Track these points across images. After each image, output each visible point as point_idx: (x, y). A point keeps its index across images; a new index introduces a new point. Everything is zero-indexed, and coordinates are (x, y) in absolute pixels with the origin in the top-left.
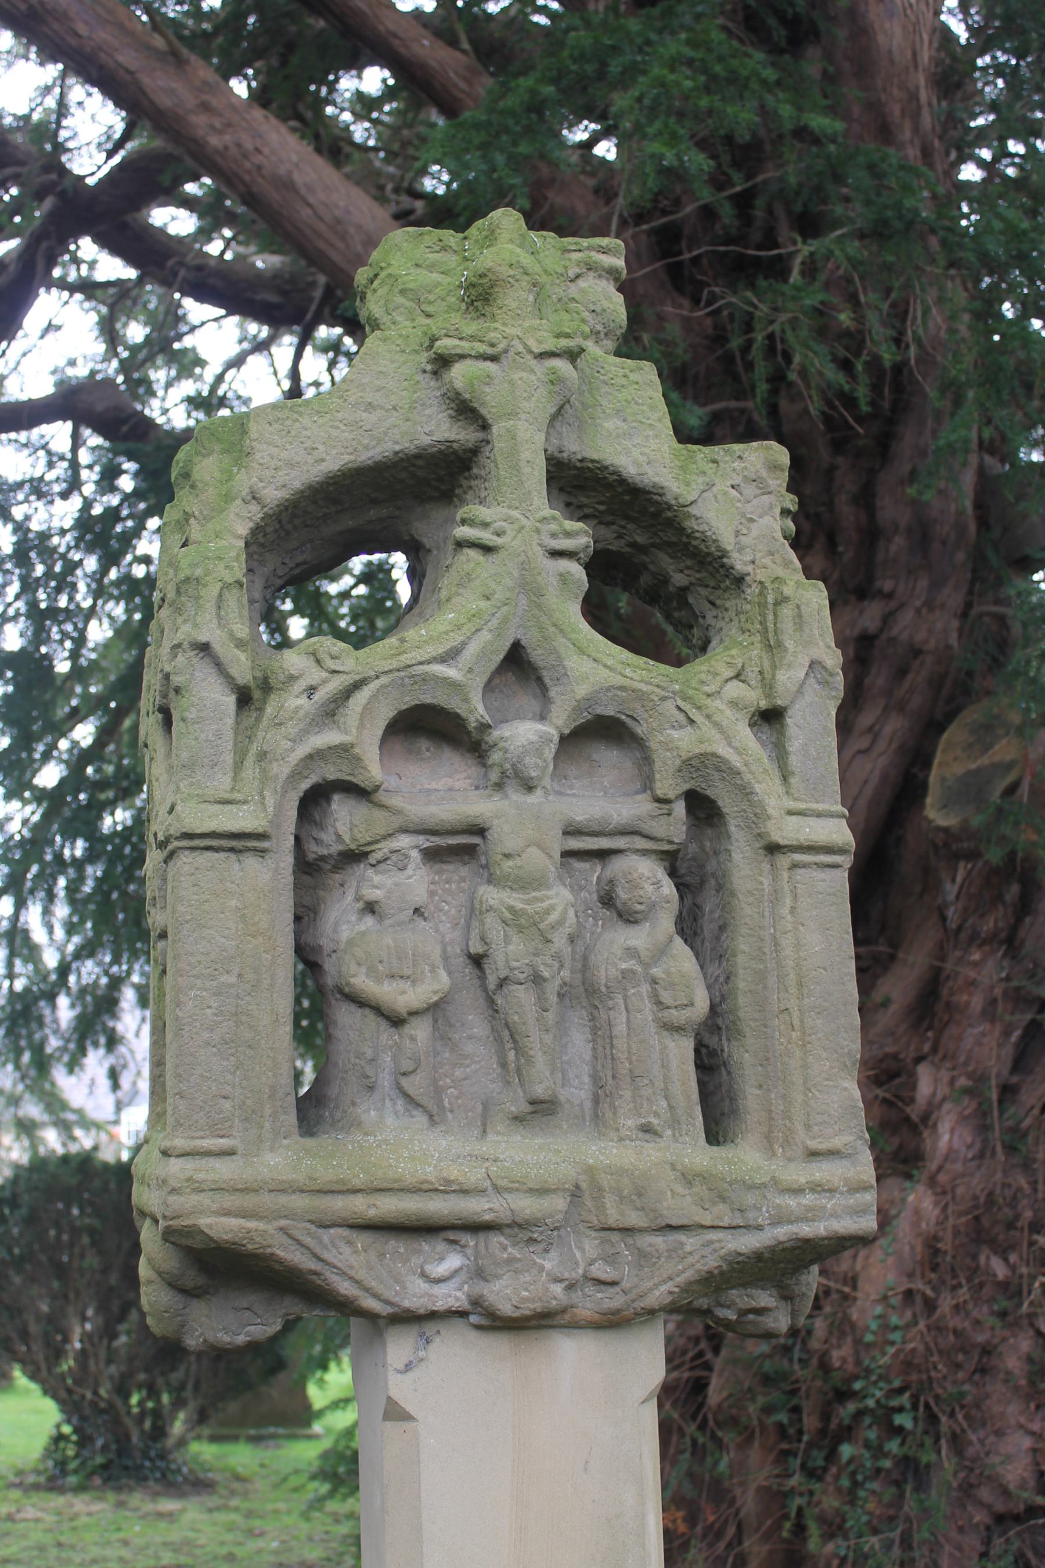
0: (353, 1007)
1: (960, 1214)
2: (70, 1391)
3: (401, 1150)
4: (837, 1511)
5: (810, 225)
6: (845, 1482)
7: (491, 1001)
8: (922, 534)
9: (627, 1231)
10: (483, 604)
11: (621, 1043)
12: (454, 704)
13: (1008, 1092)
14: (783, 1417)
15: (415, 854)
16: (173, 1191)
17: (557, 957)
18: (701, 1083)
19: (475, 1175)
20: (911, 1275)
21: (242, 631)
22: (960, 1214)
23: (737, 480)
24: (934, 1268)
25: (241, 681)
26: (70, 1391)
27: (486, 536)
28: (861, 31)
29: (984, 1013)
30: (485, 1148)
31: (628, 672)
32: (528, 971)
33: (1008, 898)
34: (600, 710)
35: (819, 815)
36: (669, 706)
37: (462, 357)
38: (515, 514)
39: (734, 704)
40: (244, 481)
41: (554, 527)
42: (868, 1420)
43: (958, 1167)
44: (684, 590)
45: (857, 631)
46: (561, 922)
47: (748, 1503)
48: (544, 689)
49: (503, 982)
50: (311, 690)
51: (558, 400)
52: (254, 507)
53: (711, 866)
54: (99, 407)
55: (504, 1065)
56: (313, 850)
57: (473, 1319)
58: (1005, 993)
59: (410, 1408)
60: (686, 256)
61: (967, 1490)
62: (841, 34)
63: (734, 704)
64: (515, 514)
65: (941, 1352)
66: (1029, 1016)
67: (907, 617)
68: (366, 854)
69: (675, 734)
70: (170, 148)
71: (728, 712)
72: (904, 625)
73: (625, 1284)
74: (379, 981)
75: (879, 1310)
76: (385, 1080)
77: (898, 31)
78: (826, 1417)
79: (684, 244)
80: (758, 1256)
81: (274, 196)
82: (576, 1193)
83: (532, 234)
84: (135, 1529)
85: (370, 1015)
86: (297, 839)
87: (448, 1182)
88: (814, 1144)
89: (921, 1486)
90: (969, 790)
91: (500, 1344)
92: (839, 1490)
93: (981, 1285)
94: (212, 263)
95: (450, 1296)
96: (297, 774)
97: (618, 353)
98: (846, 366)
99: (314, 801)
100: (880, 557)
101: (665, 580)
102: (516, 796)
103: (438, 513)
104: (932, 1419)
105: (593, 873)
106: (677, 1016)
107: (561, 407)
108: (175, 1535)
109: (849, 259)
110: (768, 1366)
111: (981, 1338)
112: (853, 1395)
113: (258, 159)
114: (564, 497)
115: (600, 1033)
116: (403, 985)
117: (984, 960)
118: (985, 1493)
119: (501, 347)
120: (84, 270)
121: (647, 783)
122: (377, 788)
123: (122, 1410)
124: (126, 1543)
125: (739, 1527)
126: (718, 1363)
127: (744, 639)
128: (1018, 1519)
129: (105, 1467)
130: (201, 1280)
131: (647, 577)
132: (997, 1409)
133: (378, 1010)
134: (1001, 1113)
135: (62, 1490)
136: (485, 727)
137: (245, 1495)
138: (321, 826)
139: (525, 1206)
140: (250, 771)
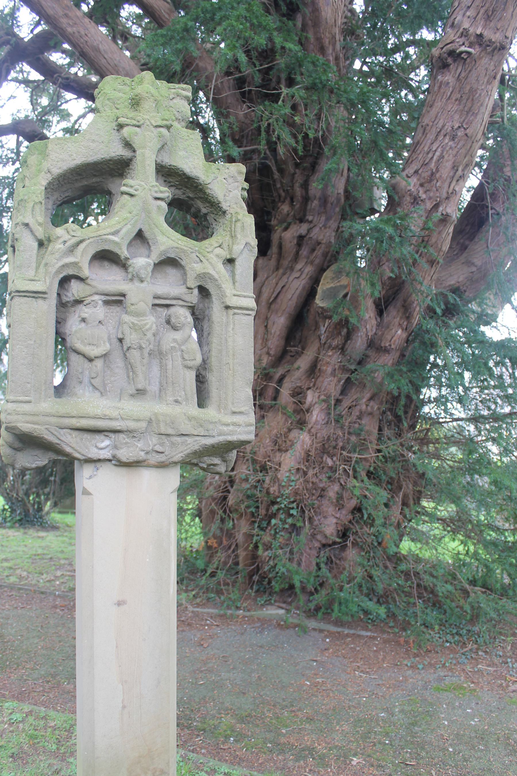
0: (76, 354)
1: (318, 443)
2: (8, 494)
3: (91, 404)
4: (269, 542)
5: (291, 82)
6: (273, 532)
7: (125, 355)
8: (324, 201)
9: (168, 435)
10: (129, 215)
11: (169, 372)
12: (116, 250)
13: (338, 402)
14: (253, 510)
15: (100, 302)
16: (9, 414)
17: (148, 340)
18: (197, 386)
19: (115, 414)
20: (299, 463)
21: (41, 219)
22: (318, 443)
23: (226, 176)
24: (308, 461)
25: (39, 238)
26: (8, 494)
27: (131, 191)
28: (316, 10)
29: (332, 373)
30: (119, 405)
31: (180, 242)
32: (138, 345)
33: (343, 333)
34: (169, 255)
35: (245, 297)
36: (194, 255)
37: (127, 125)
38: (143, 183)
39: (217, 256)
40: (46, 165)
41: (156, 189)
42: (281, 512)
43: (319, 427)
44: (206, 215)
45: (298, 234)
46: (150, 329)
47: (240, 538)
48: (150, 246)
49: (129, 348)
50: (65, 242)
51: (162, 143)
52: (49, 175)
53: (207, 313)
54: (27, 130)
55: (128, 377)
56: (65, 299)
57: (113, 462)
58: (340, 366)
59: (90, 491)
60: (247, 89)
61: (313, 536)
62: (307, 11)
63: (217, 256)
64: (143, 183)
65: (307, 489)
66: (347, 376)
67: (316, 230)
68: (83, 301)
69: (195, 265)
70: (52, 30)
71: (215, 259)
72: (315, 234)
73: (166, 453)
74: (85, 346)
75: (287, 474)
76: (86, 380)
77: (330, 11)
78: (267, 510)
79: (246, 85)
80: (213, 446)
81: (92, 54)
82: (150, 422)
83: (157, 81)
84: (29, 542)
85: (82, 358)
86: (59, 295)
87: (105, 415)
88: (235, 410)
89: (298, 534)
90: (331, 293)
91: (123, 471)
92: (271, 535)
93: (323, 468)
94: (72, 77)
95: (106, 454)
96: (58, 272)
97: (187, 128)
98: (295, 136)
99: (64, 281)
100: (309, 207)
101: (200, 211)
102: (137, 283)
103: (117, 181)
104: (303, 512)
105: (164, 312)
106: (190, 363)
107: (163, 146)
108: (43, 544)
109: (300, 97)
110: (249, 492)
111: (321, 485)
112: (277, 503)
113: (86, 38)
114: (164, 178)
115: (163, 368)
116: (91, 347)
117: (333, 355)
118: (319, 537)
119: (141, 122)
120: (25, 75)
121: (185, 282)
122: (87, 278)
123: (27, 501)
124: (26, 546)
125: (237, 545)
126: (232, 491)
127: (224, 233)
128: (330, 546)
129: (20, 520)
130: (20, 445)
131: (191, 209)
132: (325, 509)
133: (84, 356)
134: (335, 409)
135: (5, 528)
136: (127, 259)
137: (70, 531)
138: (67, 290)
139: (132, 425)
140: (42, 270)
